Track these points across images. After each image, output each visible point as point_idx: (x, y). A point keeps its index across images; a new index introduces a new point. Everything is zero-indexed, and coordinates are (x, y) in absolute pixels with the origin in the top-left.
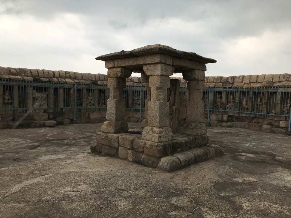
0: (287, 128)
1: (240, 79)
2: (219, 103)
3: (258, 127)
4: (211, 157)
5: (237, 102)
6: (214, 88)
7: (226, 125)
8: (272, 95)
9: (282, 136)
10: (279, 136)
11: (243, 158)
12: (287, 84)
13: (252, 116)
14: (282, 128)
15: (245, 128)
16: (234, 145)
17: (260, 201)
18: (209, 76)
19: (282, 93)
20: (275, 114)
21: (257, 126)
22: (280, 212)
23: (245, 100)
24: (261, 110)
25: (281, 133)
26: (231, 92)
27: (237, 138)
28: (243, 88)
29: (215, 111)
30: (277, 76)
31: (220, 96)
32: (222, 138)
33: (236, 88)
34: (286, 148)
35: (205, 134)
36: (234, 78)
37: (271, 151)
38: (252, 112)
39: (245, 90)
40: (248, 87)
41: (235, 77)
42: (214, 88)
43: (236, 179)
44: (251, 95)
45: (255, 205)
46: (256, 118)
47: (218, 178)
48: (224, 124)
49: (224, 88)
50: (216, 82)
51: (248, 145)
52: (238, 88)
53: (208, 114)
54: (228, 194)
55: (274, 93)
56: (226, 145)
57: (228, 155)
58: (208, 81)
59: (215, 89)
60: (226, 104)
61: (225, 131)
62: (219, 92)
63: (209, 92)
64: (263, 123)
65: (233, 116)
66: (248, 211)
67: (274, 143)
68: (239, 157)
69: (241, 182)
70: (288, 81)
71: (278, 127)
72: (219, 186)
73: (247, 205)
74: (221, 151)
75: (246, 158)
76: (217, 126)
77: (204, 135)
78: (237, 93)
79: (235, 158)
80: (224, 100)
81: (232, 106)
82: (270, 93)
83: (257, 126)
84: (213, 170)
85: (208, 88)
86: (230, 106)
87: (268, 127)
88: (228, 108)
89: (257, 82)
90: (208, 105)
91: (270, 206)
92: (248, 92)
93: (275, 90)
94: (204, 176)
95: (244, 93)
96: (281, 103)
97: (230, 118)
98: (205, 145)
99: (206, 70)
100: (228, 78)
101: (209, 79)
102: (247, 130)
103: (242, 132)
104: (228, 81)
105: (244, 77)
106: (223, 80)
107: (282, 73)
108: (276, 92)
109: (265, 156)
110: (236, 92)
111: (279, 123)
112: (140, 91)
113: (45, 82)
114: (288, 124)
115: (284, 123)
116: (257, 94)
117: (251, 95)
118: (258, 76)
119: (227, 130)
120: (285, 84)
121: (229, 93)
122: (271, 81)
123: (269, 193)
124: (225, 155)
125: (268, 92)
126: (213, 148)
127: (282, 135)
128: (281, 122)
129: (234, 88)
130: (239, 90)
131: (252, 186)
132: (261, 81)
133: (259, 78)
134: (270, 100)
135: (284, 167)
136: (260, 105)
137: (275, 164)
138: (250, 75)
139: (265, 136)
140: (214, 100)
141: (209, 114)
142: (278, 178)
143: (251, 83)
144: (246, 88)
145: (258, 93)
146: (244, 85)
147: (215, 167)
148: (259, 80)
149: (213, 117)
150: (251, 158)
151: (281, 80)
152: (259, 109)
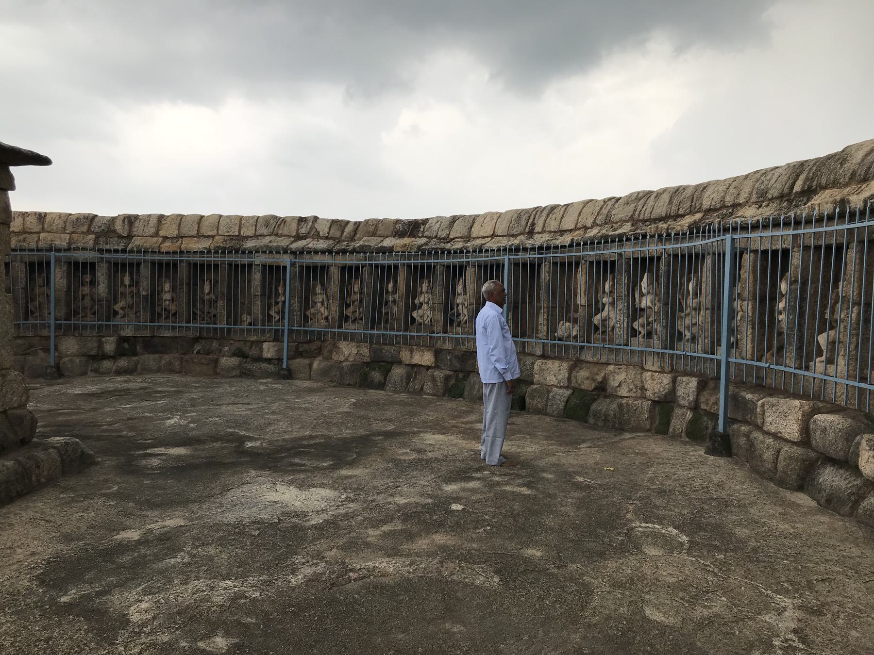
0: (280, 360)
1: (151, 224)
2: (88, 302)
3: (208, 364)
4: (43, 480)
5: (144, 293)
6: (68, 249)
7: (114, 368)
8: (240, 271)
9: (267, 383)
10: (262, 385)
11: (155, 462)
12: (275, 244)
13: (190, 334)
14: (269, 361)
15: (172, 371)
16: (132, 428)
17: (185, 583)
18: (47, 211)
19: (264, 266)
20: (250, 324)
21: (203, 361)
22: (235, 598)
23: (167, 287)
24: (214, 316)
25: (267, 375)
26: (124, 265)
27: (145, 403)
28: (159, 252)
29: (76, 327)
30: (251, 221)
31: (88, 278)
32: (94, 410)
33: (139, 252)
34: (273, 413)
35: (23, 406)
36: (130, 220)
37: (234, 427)
38: (189, 322)
39: (165, 258)
40: (175, 249)
41: (136, 217)
42: (68, 249)
43: (119, 537)
44: (183, 271)
45: (168, 598)
46: (202, 338)
47: (60, 547)
48: (107, 364)
49: (101, 251)
50: (73, 233)
51: (172, 421)
52: (145, 252)
53: (49, 337)
54: (86, 589)
55: (243, 266)
56: (106, 431)
57: (109, 462)
58: (46, 226)
59: (68, 254)
60: (108, 301)
61: (110, 386)
62: (85, 264)
63: (48, 264)
64: (220, 351)
65: (134, 337)
66: (144, 624)
67: (248, 404)
68: (144, 462)
69: (136, 538)
70: (277, 235)
71: (259, 359)
72: (57, 574)
73: (144, 605)
74: (83, 453)
75: (165, 460)
76: (84, 374)
77: (18, 411)
78: (142, 267)
79: (129, 468)
80: (102, 288)
81: (131, 307)
82: (235, 268)
83: (203, 361)
84: (47, 521)
85: (47, 250)
86: (122, 308)
87: (234, 361)
88: (116, 313)
89: (199, 236)
90: (48, 309)
91: (212, 588)
92: (175, 264)
93: (246, 260)
94: (9, 551)
95: (164, 268)
96: (263, 294)
97: (126, 346)
98: (24, 442)
99: (12, 188)
100: (113, 220)
101: (48, 219)
102: (176, 378)
103: (161, 384)
104: (115, 231)
105: (161, 218)
106: (95, 228)
107: (261, 212)
108: (250, 265)
109: (217, 445)
110: (138, 265)
111: (261, 350)
112: (285, 268)
113: (316, 252)
114: (280, 350)
115: (274, 346)
116: (201, 269)
117: (183, 271)
118: (202, 217)
119: (119, 382)
120: (270, 244)
121: (117, 268)
122: (237, 233)
123: (212, 550)
124: (98, 463)
125: (230, 264)
126: (54, 447)
127: (269, 380)
128: (265, 345)
129: (132, 251)
130: (149, 257)
131: (168, 544)
132: (210, 233)
133: (205, 223)
134: (236, 288)
135: (263, 467)
136: (210, 301)
137: (242, 464)
138: (180, 215)
139: (225, 388)
140: (71, 292)
141: (52, 338)
142: (243, 500)
143: (182, 238)
144: (168, 253)
145: (202, 265)
146: (162, 242)
147: (53, 512)
148: (205, 231)
149: (70, 346)
150: (179, 457)
151: (259, 232)
152: (209, 313)
